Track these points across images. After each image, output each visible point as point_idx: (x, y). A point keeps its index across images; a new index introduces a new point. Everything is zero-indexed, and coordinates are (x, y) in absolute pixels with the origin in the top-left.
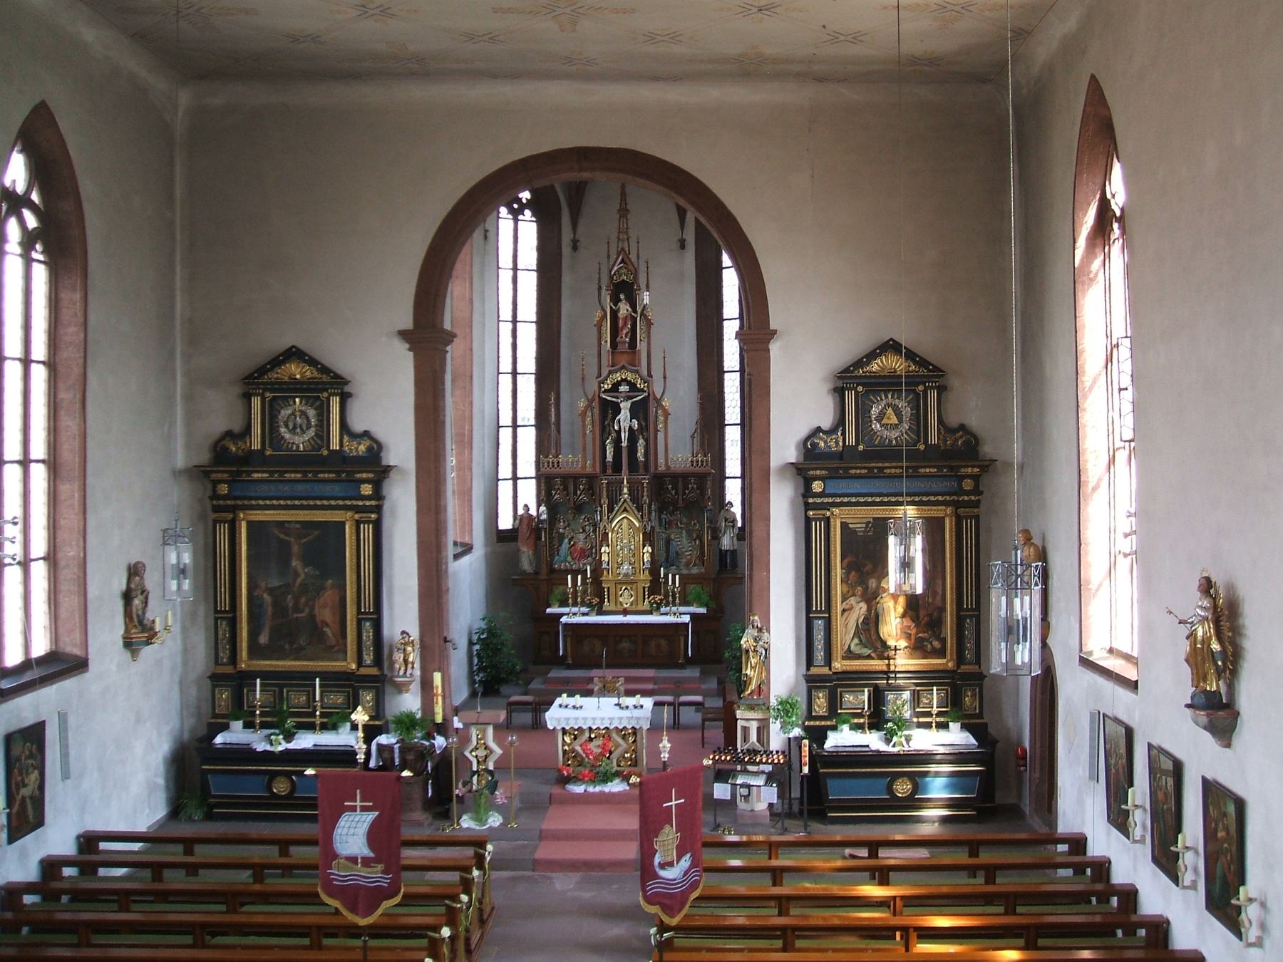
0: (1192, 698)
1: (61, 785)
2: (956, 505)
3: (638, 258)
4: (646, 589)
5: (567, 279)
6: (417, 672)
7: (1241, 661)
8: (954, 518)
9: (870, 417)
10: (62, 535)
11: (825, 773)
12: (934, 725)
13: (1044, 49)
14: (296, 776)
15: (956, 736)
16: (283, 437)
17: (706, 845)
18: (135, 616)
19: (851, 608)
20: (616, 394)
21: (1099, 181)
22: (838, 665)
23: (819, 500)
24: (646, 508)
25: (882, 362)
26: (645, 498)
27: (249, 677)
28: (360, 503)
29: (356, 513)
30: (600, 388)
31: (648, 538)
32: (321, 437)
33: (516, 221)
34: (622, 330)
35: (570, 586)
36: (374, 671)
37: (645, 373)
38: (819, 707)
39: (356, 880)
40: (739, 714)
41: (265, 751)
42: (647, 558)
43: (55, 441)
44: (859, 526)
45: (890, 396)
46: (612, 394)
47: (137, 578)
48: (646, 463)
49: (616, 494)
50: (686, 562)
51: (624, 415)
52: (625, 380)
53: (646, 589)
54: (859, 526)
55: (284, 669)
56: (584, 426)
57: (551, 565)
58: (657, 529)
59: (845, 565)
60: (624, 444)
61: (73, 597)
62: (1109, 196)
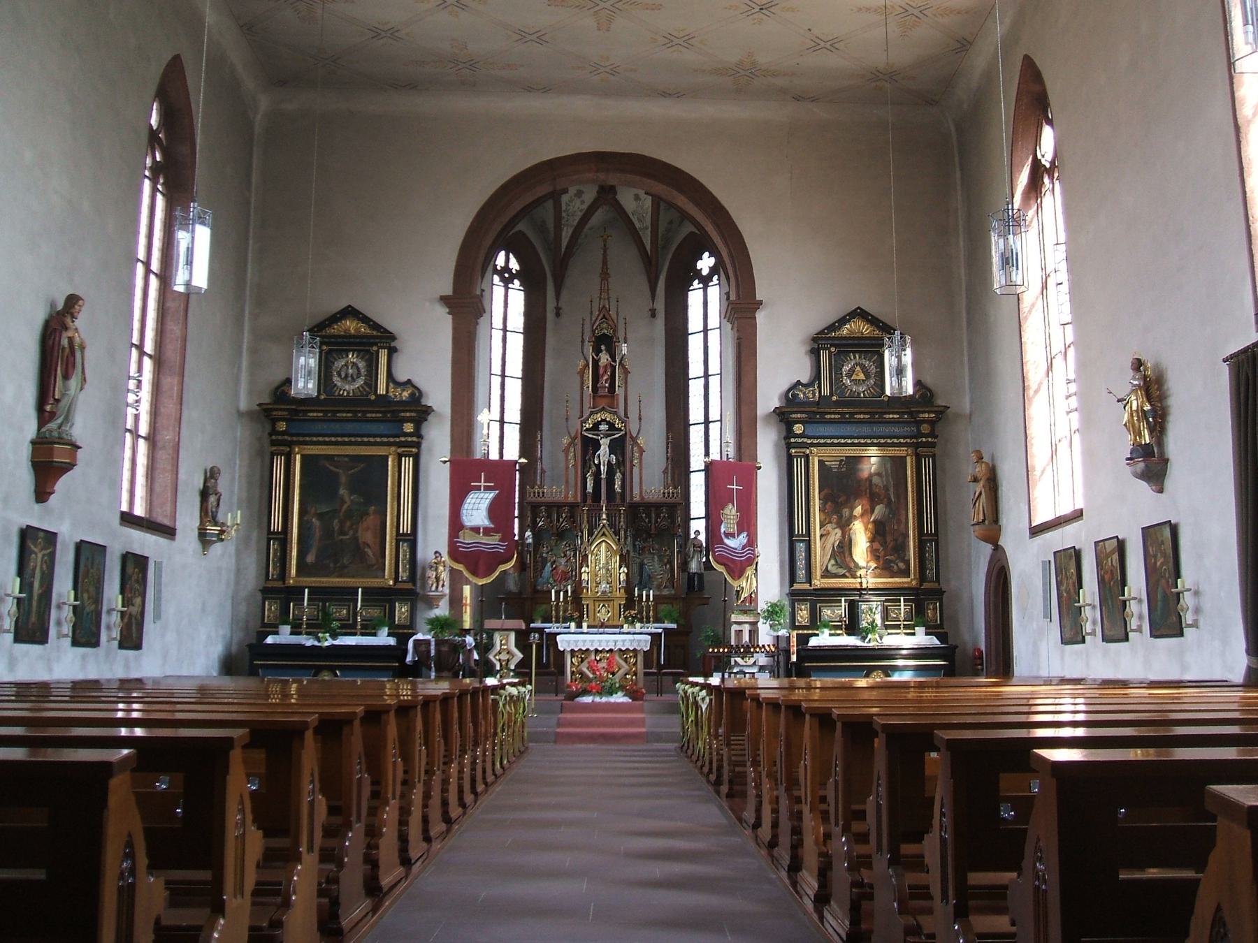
0: (1131, 453)
1: (152, 625)
2: (916, 446)
3: (617, 315)
4: (622, 606)
5: (551, 341)
6: (447, 590)
7: (1166, 423)
8: (914, 457)
9: (841, 374)
10: (161, 421)
11: (808, 666)
12: (902, 626)
13: (979, 61)
14: (340, 671)
15: (921, 638)
16: (335, 385)
17: (495, 775)
18: (210, 511)
20: (596, 432)
21: (1031, 147)
22: (818, 582)
23: (800, 440)
24: (622, 533)
26: (622, 523)
27: (296, 592)
28: (403, 439)
29: (399, 447)
30: (582, 426)
31: (624, 560)
33: (507, 288)
34: (603, 376)
35: (553, 599)
36: (410, 586)
37: (622, 413)
38: (801, 617)
39: (478, 547)
40: (734, 618)
41: (313, 645)
42: (623, 577)
43: (161, 342)
44: (833, 463)
45: (857, 357)
46: (592, 432)
47: (213, 481)
48: (623, 494)
49: (596, 520)
50: (657, 585)
51: (604, 450)
52: (605, 420)
53: (622, 606)
54: (833, 463)
55: (327, 585)
56: (567, 460)
57: (535, 586)
58: (632, 554)
59: (822, 497)
60: (603, 476)
61: (167, 474)
62: (1039, 157)
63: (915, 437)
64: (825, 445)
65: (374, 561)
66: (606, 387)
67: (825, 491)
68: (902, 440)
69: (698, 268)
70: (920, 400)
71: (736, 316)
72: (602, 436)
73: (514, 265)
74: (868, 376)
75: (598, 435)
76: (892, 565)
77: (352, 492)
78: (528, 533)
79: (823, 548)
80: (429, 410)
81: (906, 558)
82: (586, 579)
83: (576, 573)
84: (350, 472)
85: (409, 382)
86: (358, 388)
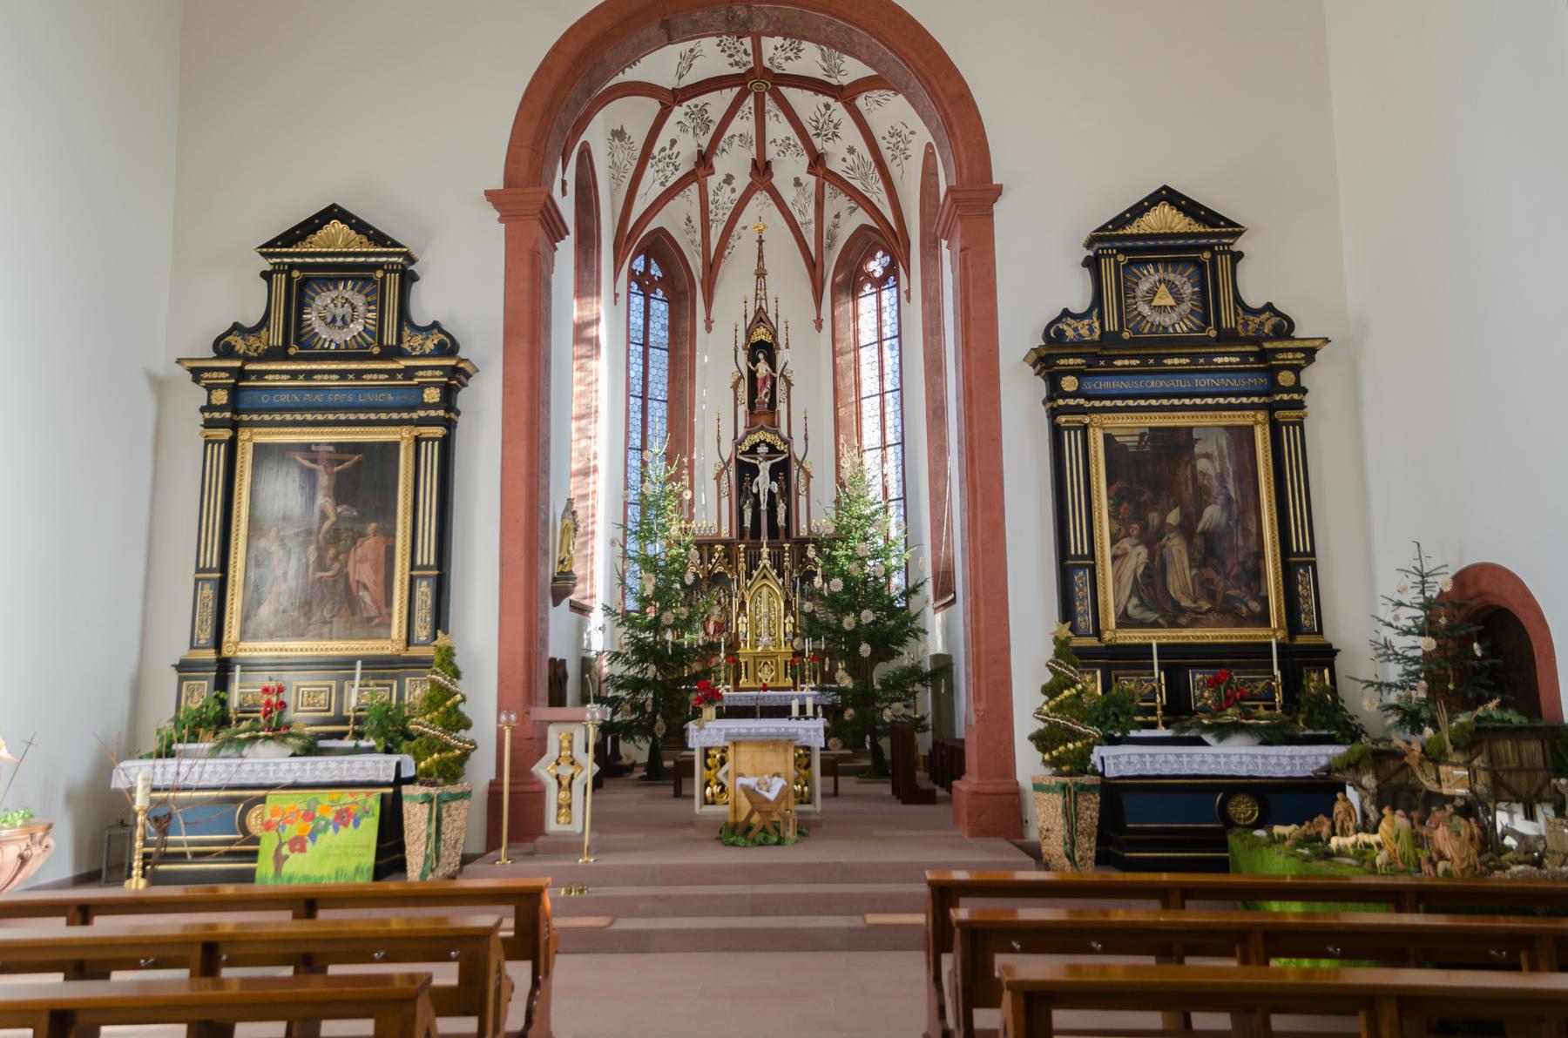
2: (1271, 408)
3: (777, 316)
19: (1125, 554)
22: (1114, 634)
23: (1071, 402)
42: (789, 628)
52: (764, 441)
63: (1268, 394)
65: (373, 611)
66: (764, 402)
67: (1117, 485)
70: (1271, 335)
71: (958, 212)
73: (656, 271)
74: (1179, 299)
75: (756, 459)
79: (1117, 578)
81: (1262, 594)
82: (744, 630)
84: (336, 469)
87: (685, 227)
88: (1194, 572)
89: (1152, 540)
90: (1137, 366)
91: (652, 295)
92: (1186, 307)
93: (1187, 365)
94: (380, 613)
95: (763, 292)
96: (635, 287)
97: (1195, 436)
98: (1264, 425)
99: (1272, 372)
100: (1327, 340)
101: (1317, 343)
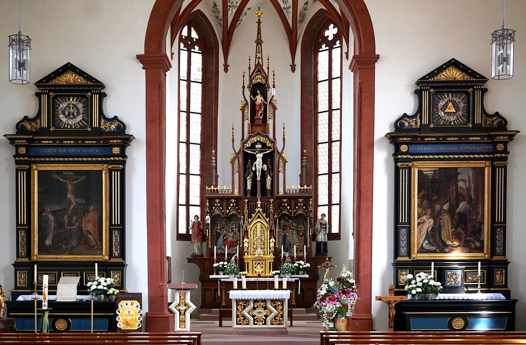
2: (492, 160)
3: (268, 68)
4: (271, 264)
9: (437, 108)
16: (61, 121)
19: (424, 222)
22: (416, 256)
23: (405, 157)
25: (446, 73)
28: (112, 159)
30: (243, 146)
32: (86, 121)
34: (258, 112)
36: (120, 260)
42: (272, 245)
44: (429, 172)
45: (450, 96)
52: (260, 141)
53: (271, 264)
54: (429, 172)
59: (420, 196)
60: (259, 179)
63: (492, 154)
64: (424, 159)
65: (94, 243)
66: (260, 119)
68: (482, 156)
69: (326, 35)
72: (257, 152)
73: (194, 35)
75: (255, 151)
76: (471, 243)
77: (76, 196)
78: (208, 217)
79: (420, 232)
80: (131, 138)
82: (247, 246)
83: (240, 242)
84: (74, 182)
85: (116, 117)
86: (78, 122)
87: (213, 9)
88: (453, 230)
89: (436, 216)
90: (435, 140)
91: (192, 50)
92: (460, 113)
93: (457, 140)
94: (97, 244)
95: (260, 55)
96: (182, 45)
97: (458, 172)
98: (489, 167)
99: (495, 144)
100: (518, 132)
101: (513, 133)
